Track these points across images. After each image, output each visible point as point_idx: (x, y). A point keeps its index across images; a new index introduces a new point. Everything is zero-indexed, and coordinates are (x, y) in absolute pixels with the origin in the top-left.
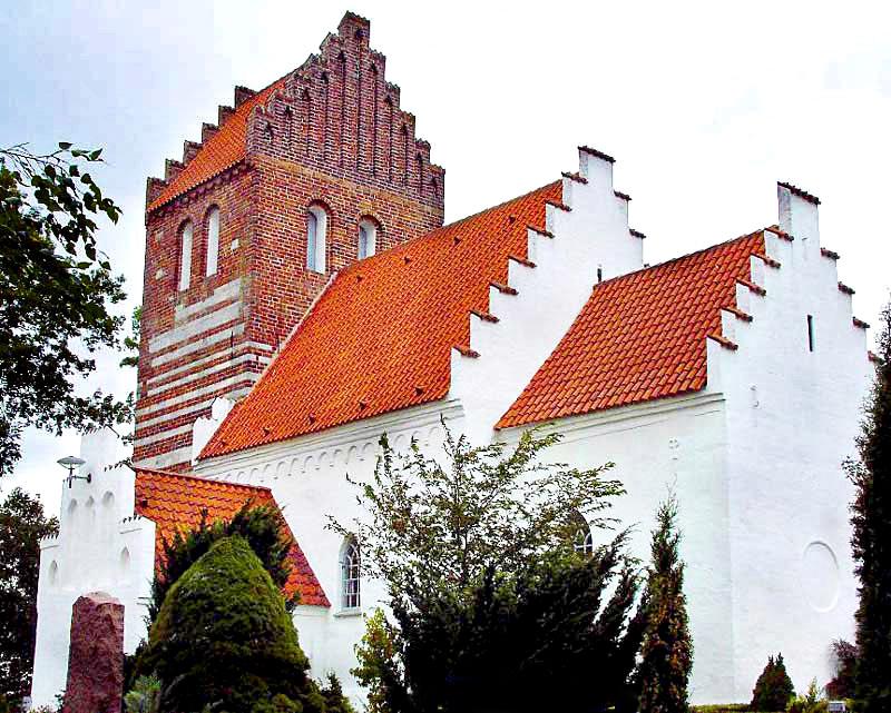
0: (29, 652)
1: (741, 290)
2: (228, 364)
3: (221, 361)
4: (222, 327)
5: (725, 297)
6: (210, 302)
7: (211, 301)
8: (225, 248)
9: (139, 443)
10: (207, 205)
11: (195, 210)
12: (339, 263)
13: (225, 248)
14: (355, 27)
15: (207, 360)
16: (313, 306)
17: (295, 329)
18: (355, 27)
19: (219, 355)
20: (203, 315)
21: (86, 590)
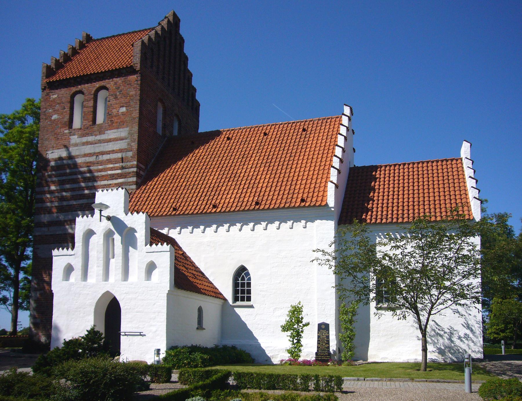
1: (228, 225)
2: (119, 171)
3: (112, 169)
4: (113, 152)
10: (98, 86)
11: (90, 88)
15: (100, 167)
19: (111, 166)
20: (96, 144)
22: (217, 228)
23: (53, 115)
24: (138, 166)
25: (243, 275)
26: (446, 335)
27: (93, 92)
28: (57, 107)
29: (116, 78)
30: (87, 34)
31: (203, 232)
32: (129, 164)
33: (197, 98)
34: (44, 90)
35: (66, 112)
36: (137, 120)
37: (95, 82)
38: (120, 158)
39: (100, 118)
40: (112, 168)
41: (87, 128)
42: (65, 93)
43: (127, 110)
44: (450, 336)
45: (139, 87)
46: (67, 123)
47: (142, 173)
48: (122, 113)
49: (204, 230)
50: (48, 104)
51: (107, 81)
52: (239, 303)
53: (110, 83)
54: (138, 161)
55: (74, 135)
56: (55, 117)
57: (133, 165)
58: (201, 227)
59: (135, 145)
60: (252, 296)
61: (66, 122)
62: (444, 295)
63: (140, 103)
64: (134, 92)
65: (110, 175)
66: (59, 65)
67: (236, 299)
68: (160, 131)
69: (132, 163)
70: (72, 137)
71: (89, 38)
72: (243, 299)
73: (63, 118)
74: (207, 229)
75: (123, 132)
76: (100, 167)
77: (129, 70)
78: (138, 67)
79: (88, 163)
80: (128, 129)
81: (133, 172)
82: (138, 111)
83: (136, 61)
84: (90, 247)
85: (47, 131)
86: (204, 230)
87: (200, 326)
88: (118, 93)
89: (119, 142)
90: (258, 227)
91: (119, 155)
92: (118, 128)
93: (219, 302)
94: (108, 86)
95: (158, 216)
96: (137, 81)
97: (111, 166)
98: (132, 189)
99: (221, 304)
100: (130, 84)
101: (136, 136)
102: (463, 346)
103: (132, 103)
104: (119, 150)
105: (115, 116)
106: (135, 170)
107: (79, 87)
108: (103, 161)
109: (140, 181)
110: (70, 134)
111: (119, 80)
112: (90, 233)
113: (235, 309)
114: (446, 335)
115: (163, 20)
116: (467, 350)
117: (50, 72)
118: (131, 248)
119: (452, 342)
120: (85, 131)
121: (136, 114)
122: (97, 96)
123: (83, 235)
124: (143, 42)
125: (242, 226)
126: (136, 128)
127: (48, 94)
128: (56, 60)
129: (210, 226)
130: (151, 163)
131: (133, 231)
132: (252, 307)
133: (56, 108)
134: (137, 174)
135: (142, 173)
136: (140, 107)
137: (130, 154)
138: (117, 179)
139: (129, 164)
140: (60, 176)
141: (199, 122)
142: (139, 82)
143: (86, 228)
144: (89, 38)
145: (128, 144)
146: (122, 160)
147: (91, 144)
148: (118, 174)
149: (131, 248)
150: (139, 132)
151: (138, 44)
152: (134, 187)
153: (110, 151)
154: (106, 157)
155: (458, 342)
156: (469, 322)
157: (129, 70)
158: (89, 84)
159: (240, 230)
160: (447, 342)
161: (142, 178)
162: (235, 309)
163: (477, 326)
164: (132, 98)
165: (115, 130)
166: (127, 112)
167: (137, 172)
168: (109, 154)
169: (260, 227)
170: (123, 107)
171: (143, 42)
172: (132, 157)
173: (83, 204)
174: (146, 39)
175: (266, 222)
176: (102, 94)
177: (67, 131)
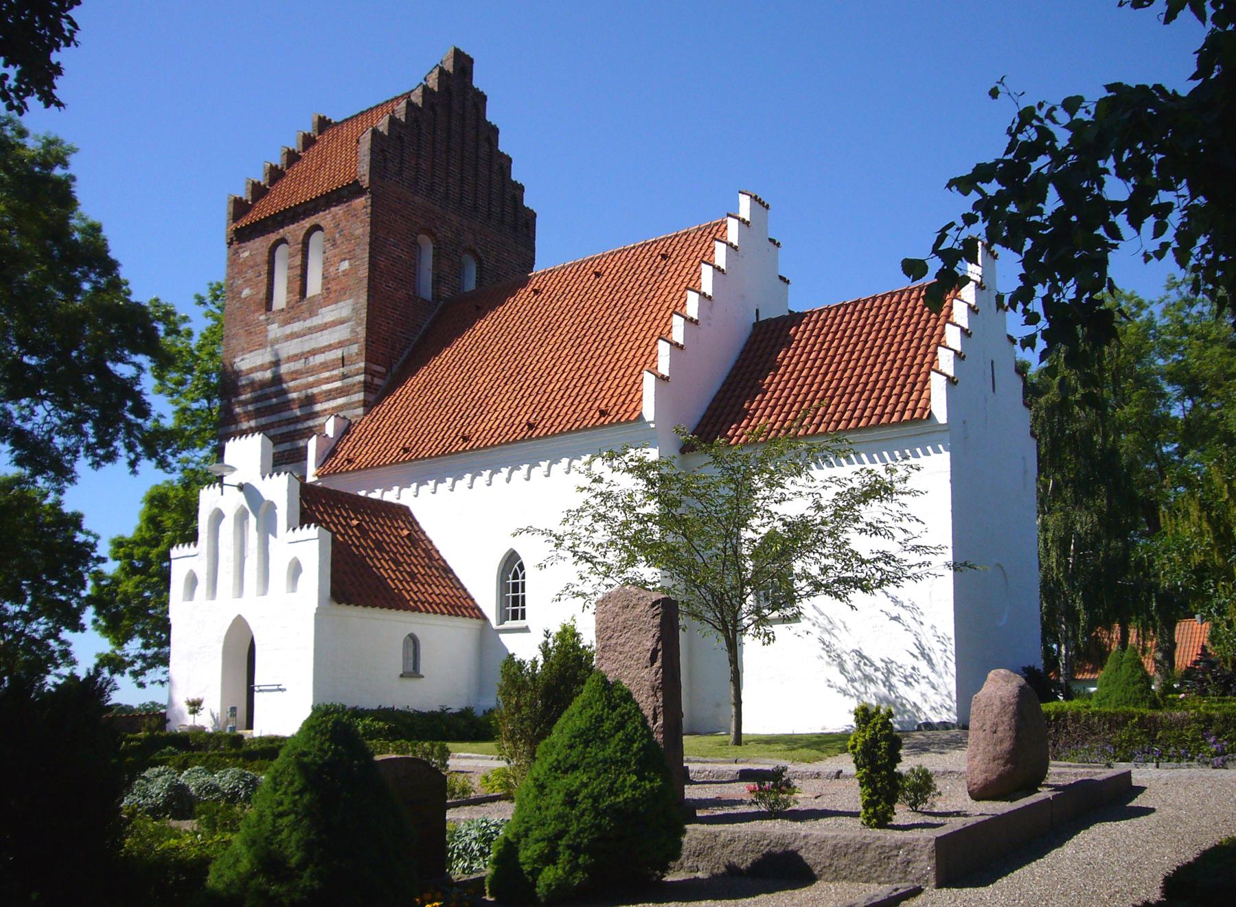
0: (527, 228)
1: (489, 472)
2: (338, 384)
3: (328, 380)
4: (330, 348)
5: (758, 349)
6: (316, 321)
7: (316, 321)
8: (332, 269)
9: (259, 405)
10: (308, 226)
11: (295, 231)
12: (446, 292)
13: (332, 269)
14: (463, 63)
15: (311, 379)
16: (420, 333)
17: (406, 353)
18: (463, 63)
19: (327, 374)
20: (305, 335)
21: (114, 536)
22: (473, 479)
23: (243, 289)
24: (367, 371)
25: (516, 570)
26: (879, 674)
27: (301, 237)
28: (250, 274)
29: (336, 206)
30: (319, 117)
31: (452, 490)
32: (353, 368)
33: (526, 204)
34: (230, 244)
35: (261, 281)
36: (366, 281)
37: (303, 219)
38: (338, 359)
39: (314, 286)
40: (327, 378)
41: (293, 308)
42: (257, 248)
43: (350, 265)
44: (887, 679)
45: (369, 220)
46: (264, 302)
47: (377, 381)
48: (343, 271)
49: (453, 485)
50: (236, 270)
51: (321, 213)
52: (510, 624)
53: (324, 218)
54: (367, 360)
55: (273, 323)
56: (246, 292)
57: (360, 368)
58: (448, 479)
59: (362, 331)
60: (529, 607)
61: (261, 300)
62: (885, 588)
63: (370, 248)
64: (361, 230)
65: (326, 392)
66: (259, 191)
67: (503, 618)
68: (426, 288)
69: (357, 366)
70: (269, 327)
71: (324, 124)
72: (515, 617)
73: (258, 293)
74: (458, 482)
75: (343, 309)
76: (311, 379)
77: (351, 191)
78: (365, 181)
79: (292, 373)
80: (350, 301)
81: (360, 382)
82: (367, 266)
83: (363, 170)
84: (220, 540)
85: (235, 320)
86: (453, 485)
87: (413, 671)
88: (337, 236)
89: (338, 327)
90: (535, 471)
91: (338, 353)
92: (336, 302)
93: (473, 624)
94: (322, 224)
95: (578, 429)
96: (365, 207)
97: (327, 374)
98: (357, 416)
99: (478, 627)
100: (355, 215)
101: (364, 315)
102: (911, 695)
103: (358, 252)
104: (339, 343)
105: (334, 279)
106: (361, 378)
107: (281, 231)
108: (314, 366)
109: (372, 398)
110: (269, 322)
111: (338, 210)
112: (218, 516)
113: (501, 636)
114: (879, 674)
115: (431, 72)
116: (919, 704)
117: (240, 208)
118: (271, 537)
119: (891, 687)
120: (291, 315)
121: (364, 272)
122: (308, 244)
123: (210, 520)
124: (375, 132)
125: (510, 473)
126: (363, 299)
127: (236, 252)
128: (254, 184)
129: (461, 477)
130: (401, 359)
131: (272, 506)
132: (526, 630)
133: (248, 276)
134: (365, 387)
135: (377, 381)
136: (370, 257)
137: (355, 349)
138: (336, 398)
139: (353, 368)
140: (257, 402)
141: (534, 251)
142: (369, 210)
143: (212, 509)
144: (324, 124)
145: (353, 331)
146: (343, 361)
147: (298, 337)
148: (337, 388)
149: (271, 537)
150: (369, 304)
151: (367, 138)
152: (360, 411)
153: (325, 347)
154: (320, 359)
155: (902, 689)
156: (924, 643)
157: (351, 191)
158: (296, 224)
159: (508, 480)
160: (884, 691)
161: (379, 393)
162: (501, 636)
163: (938, 647)
164: (358, 241)
165: (333, 307)
166: (350, 270)
167: (365, 382)
168: (323, 352)
169: (443, 488)
170: (344, 260)
171: (375, 132)
172: (357, 354)
173: (285, 451)
174: (383, 125)
175: (548, 461)
176: (316, 238)
177: (262, 317)
